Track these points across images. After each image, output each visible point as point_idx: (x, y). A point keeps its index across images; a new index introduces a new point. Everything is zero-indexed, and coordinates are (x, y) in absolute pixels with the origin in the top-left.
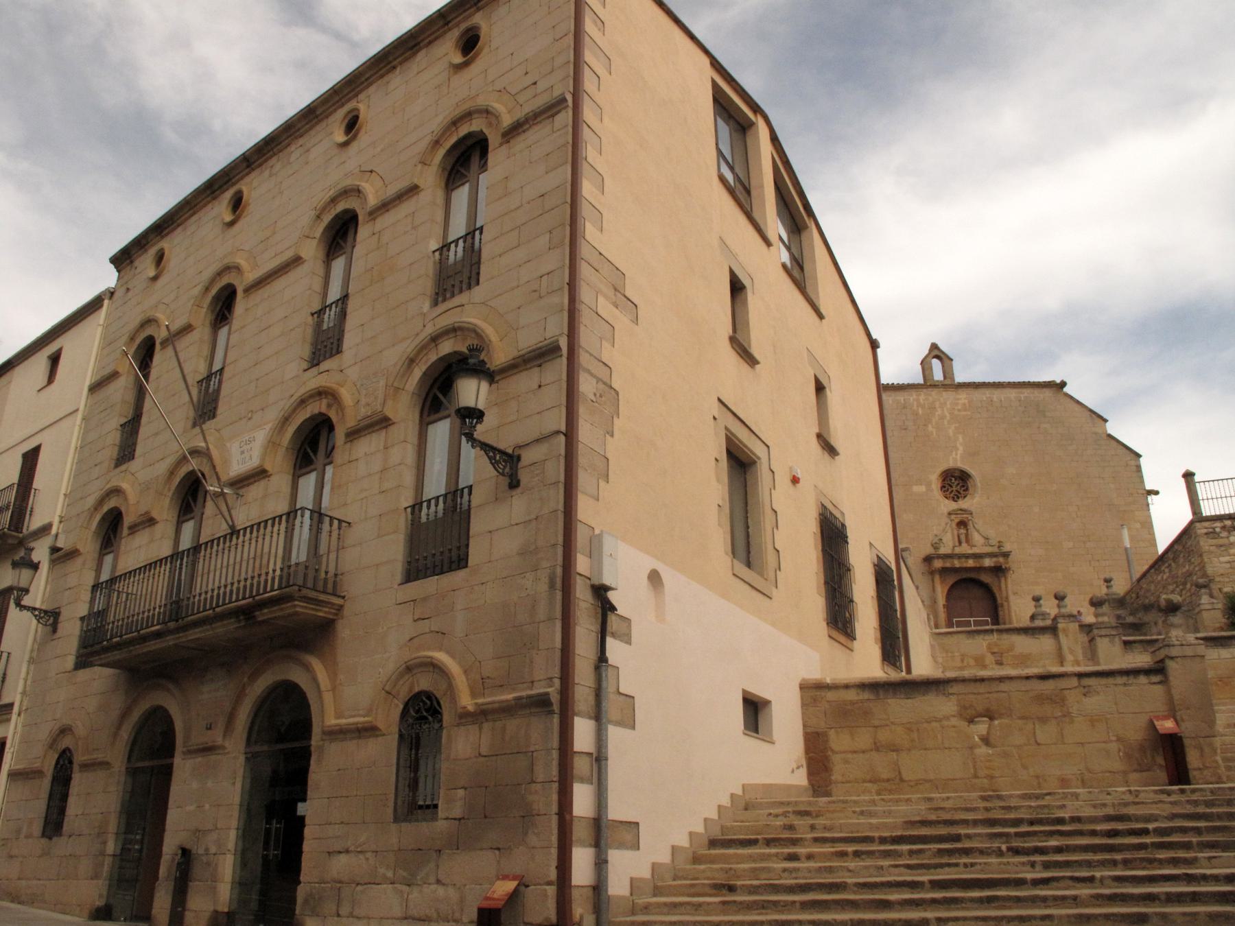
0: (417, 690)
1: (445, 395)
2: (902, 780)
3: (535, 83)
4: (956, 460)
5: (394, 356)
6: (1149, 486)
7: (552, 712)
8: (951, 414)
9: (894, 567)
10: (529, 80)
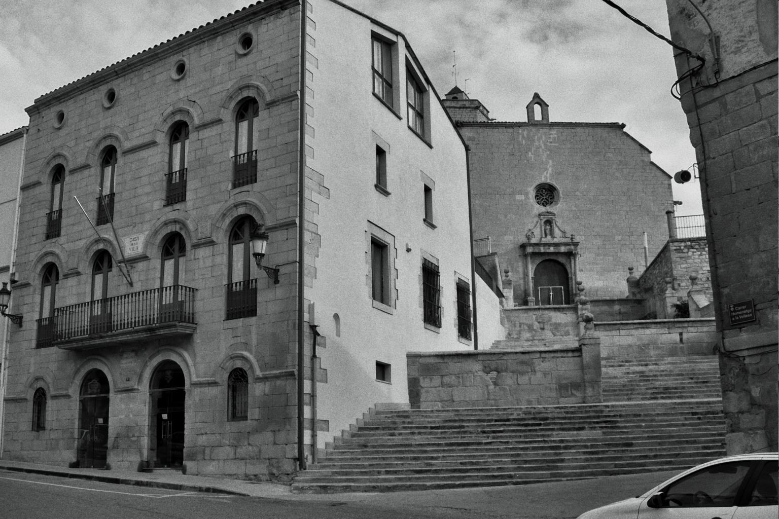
0: (235, 367)
1: (240, 230)
2: (453, 401)
3: (282, 79)
4: (546, 177)
5: (214, 210)
7: (295, 379)
8: (545, 144)
10: (279, 76)
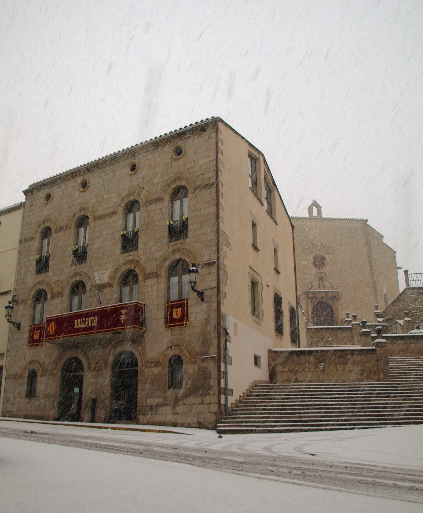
6: (398, 265)
9: (296, 309)
